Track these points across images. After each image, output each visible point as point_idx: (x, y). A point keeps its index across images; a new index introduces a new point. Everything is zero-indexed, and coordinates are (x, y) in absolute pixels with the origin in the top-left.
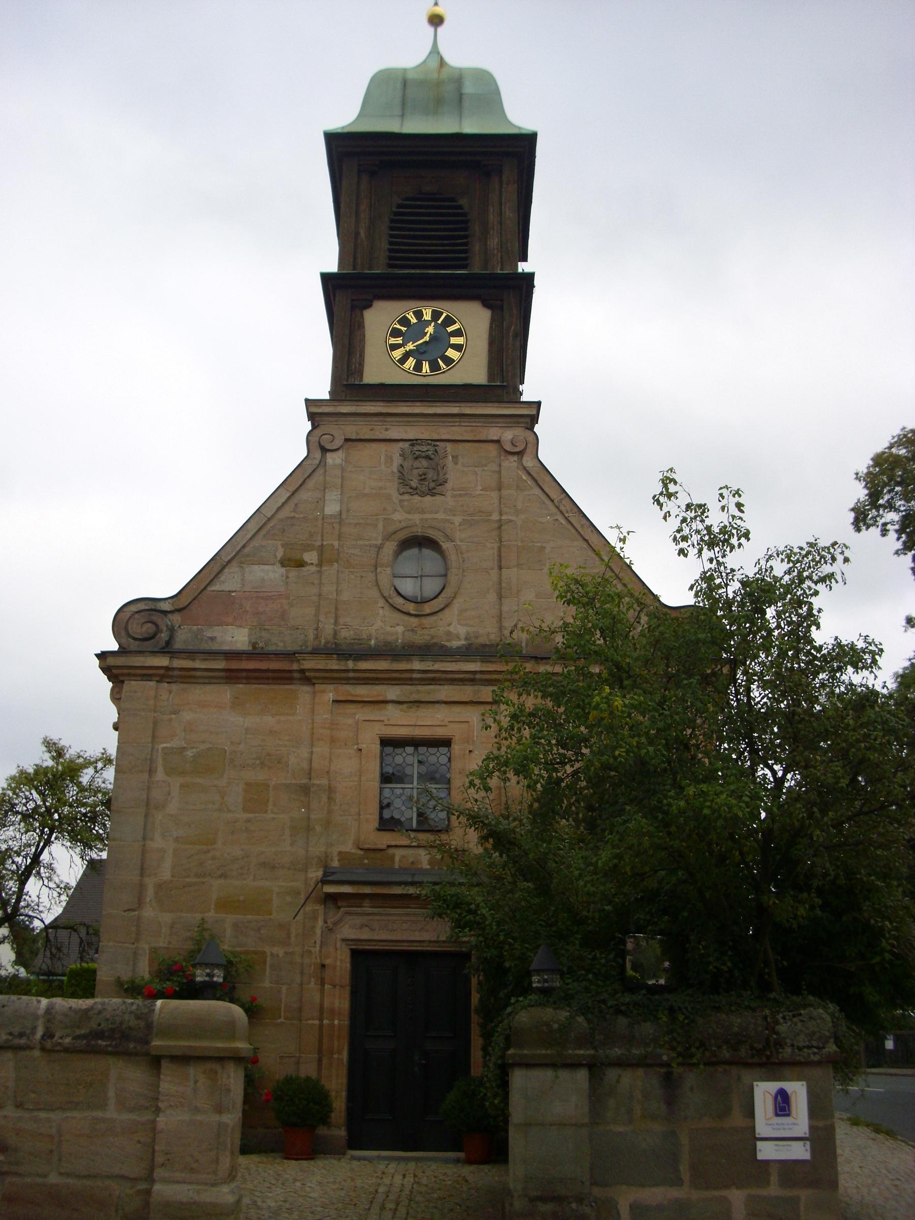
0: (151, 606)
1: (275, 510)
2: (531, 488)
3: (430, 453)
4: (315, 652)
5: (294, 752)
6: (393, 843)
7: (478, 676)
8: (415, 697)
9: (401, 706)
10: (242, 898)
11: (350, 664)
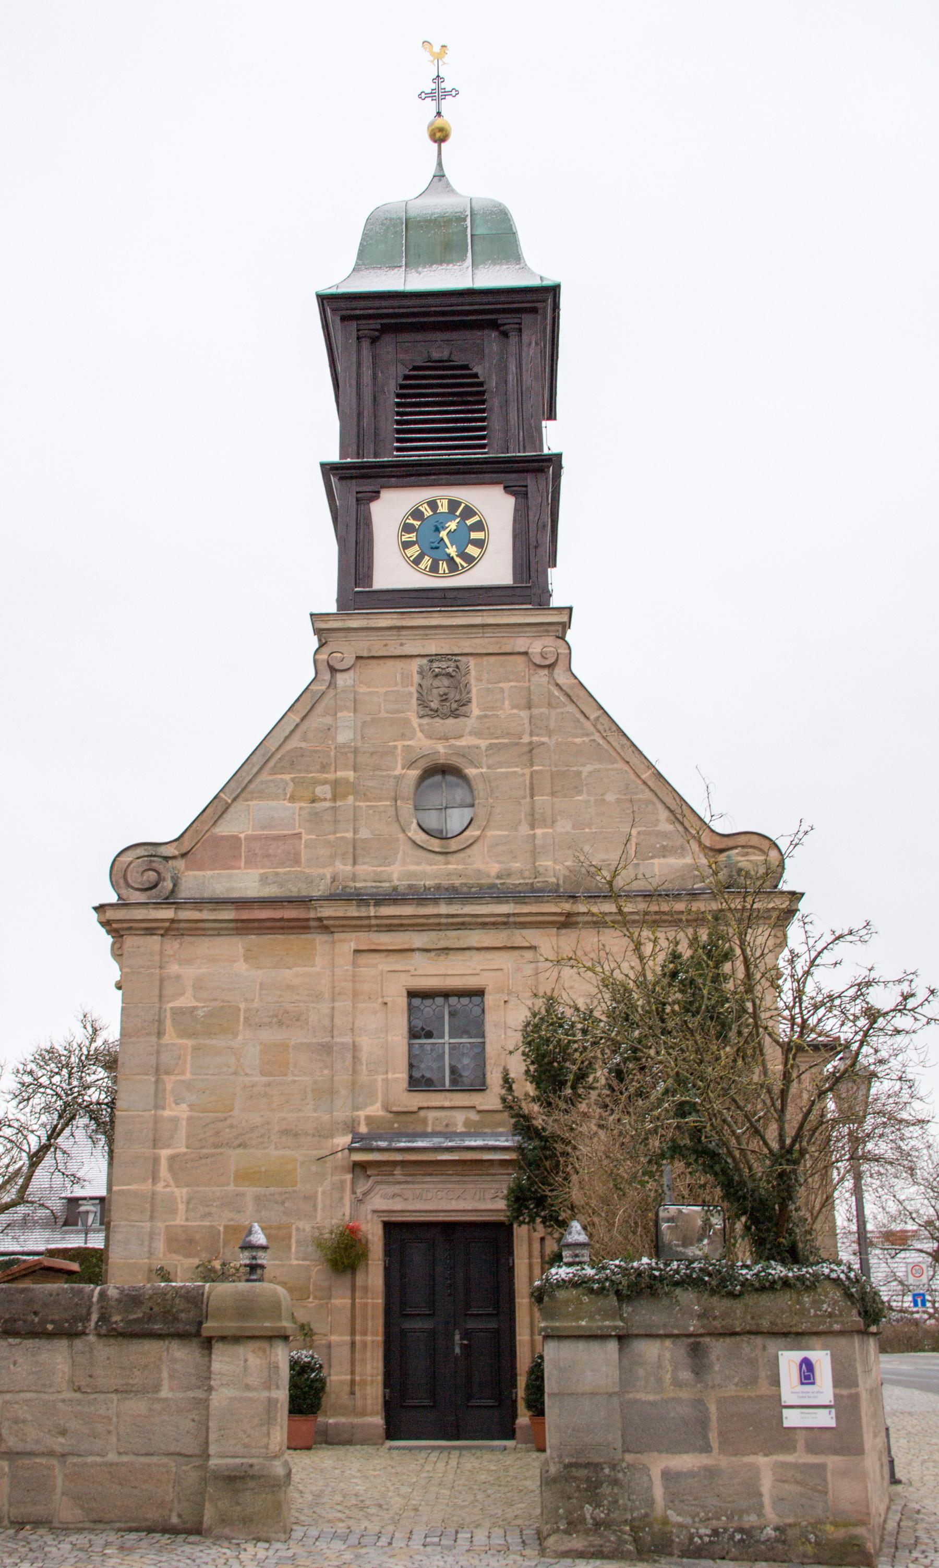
0: (151, 851)
1: (282, 740)
2: (565, 705)
3: (450, 670)
4: (332, 898)
5: (314, 1008)
6: (425, 1105)
7: (512, 919)
9: (429, 954)
10: (263, 1169)
11: (372, 911)
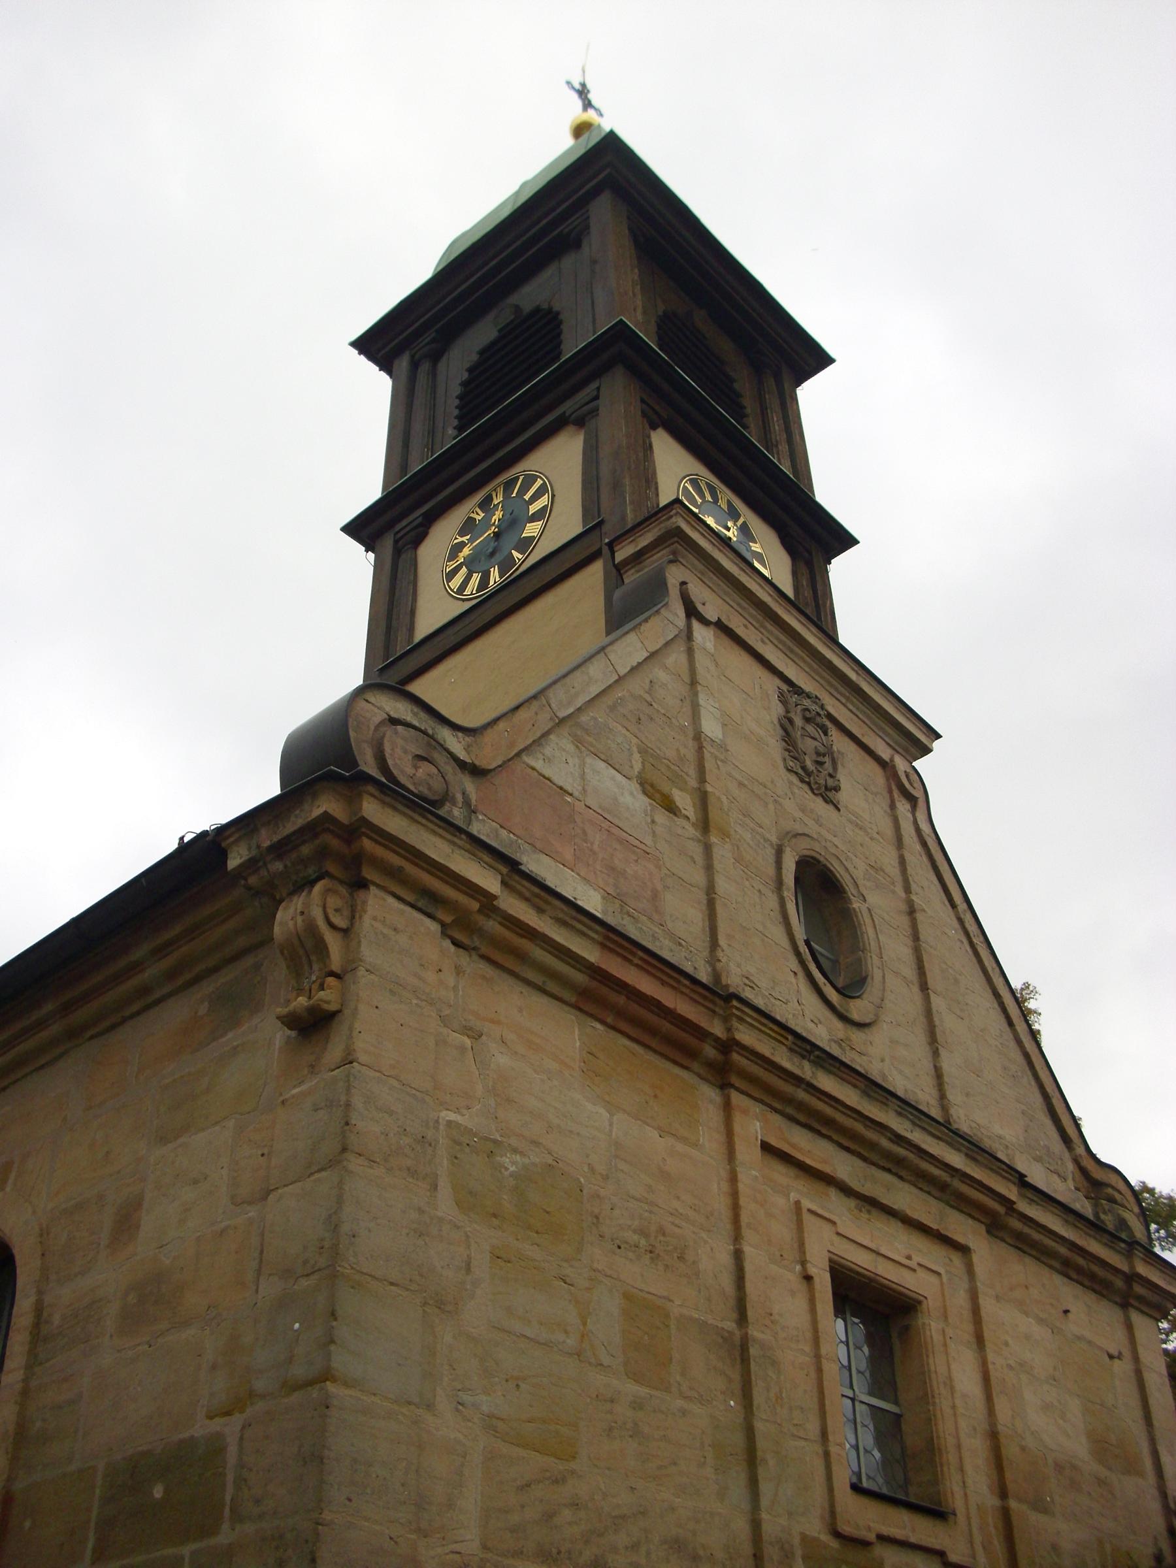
8: (867, 1189)
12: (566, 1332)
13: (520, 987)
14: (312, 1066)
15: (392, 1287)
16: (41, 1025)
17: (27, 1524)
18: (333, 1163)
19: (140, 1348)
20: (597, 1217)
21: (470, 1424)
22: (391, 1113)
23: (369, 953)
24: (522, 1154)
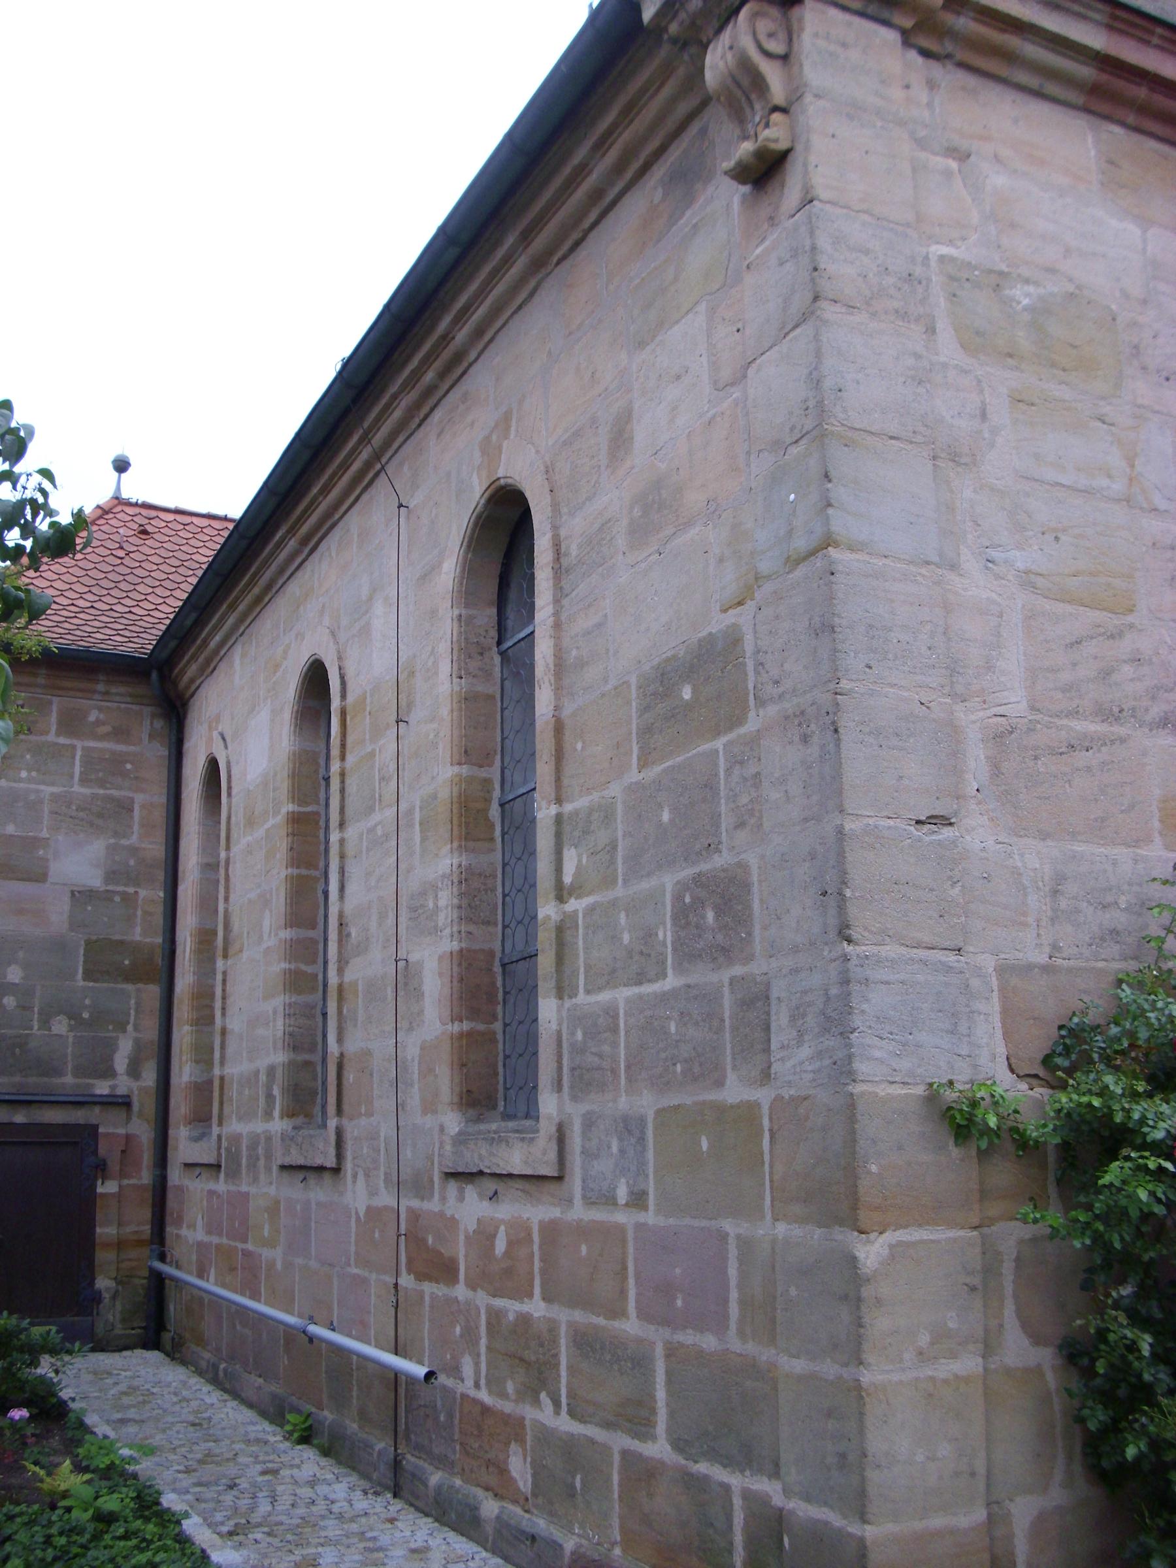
12: (1109, 476)
13: (1010, 95)
14: (771, 218)
15: (893, 441)
16: (508, 261)
17: (579, 746)
18: (804, 319)
19: (651, 558)
20: (1136, 347)
21: (1003, 582)
22: (867, 252)
23: (813, 74)
24: (1037, 284)
